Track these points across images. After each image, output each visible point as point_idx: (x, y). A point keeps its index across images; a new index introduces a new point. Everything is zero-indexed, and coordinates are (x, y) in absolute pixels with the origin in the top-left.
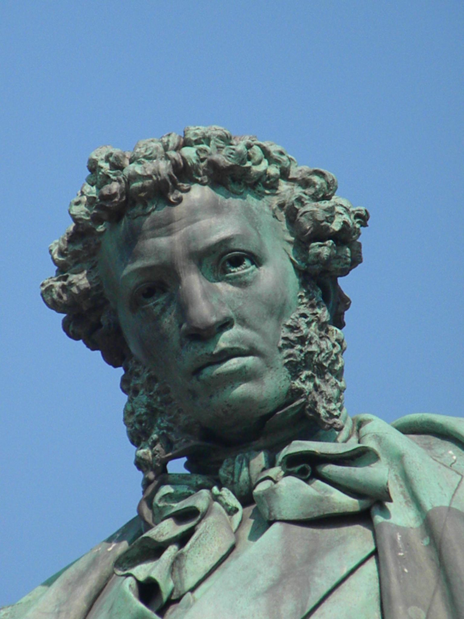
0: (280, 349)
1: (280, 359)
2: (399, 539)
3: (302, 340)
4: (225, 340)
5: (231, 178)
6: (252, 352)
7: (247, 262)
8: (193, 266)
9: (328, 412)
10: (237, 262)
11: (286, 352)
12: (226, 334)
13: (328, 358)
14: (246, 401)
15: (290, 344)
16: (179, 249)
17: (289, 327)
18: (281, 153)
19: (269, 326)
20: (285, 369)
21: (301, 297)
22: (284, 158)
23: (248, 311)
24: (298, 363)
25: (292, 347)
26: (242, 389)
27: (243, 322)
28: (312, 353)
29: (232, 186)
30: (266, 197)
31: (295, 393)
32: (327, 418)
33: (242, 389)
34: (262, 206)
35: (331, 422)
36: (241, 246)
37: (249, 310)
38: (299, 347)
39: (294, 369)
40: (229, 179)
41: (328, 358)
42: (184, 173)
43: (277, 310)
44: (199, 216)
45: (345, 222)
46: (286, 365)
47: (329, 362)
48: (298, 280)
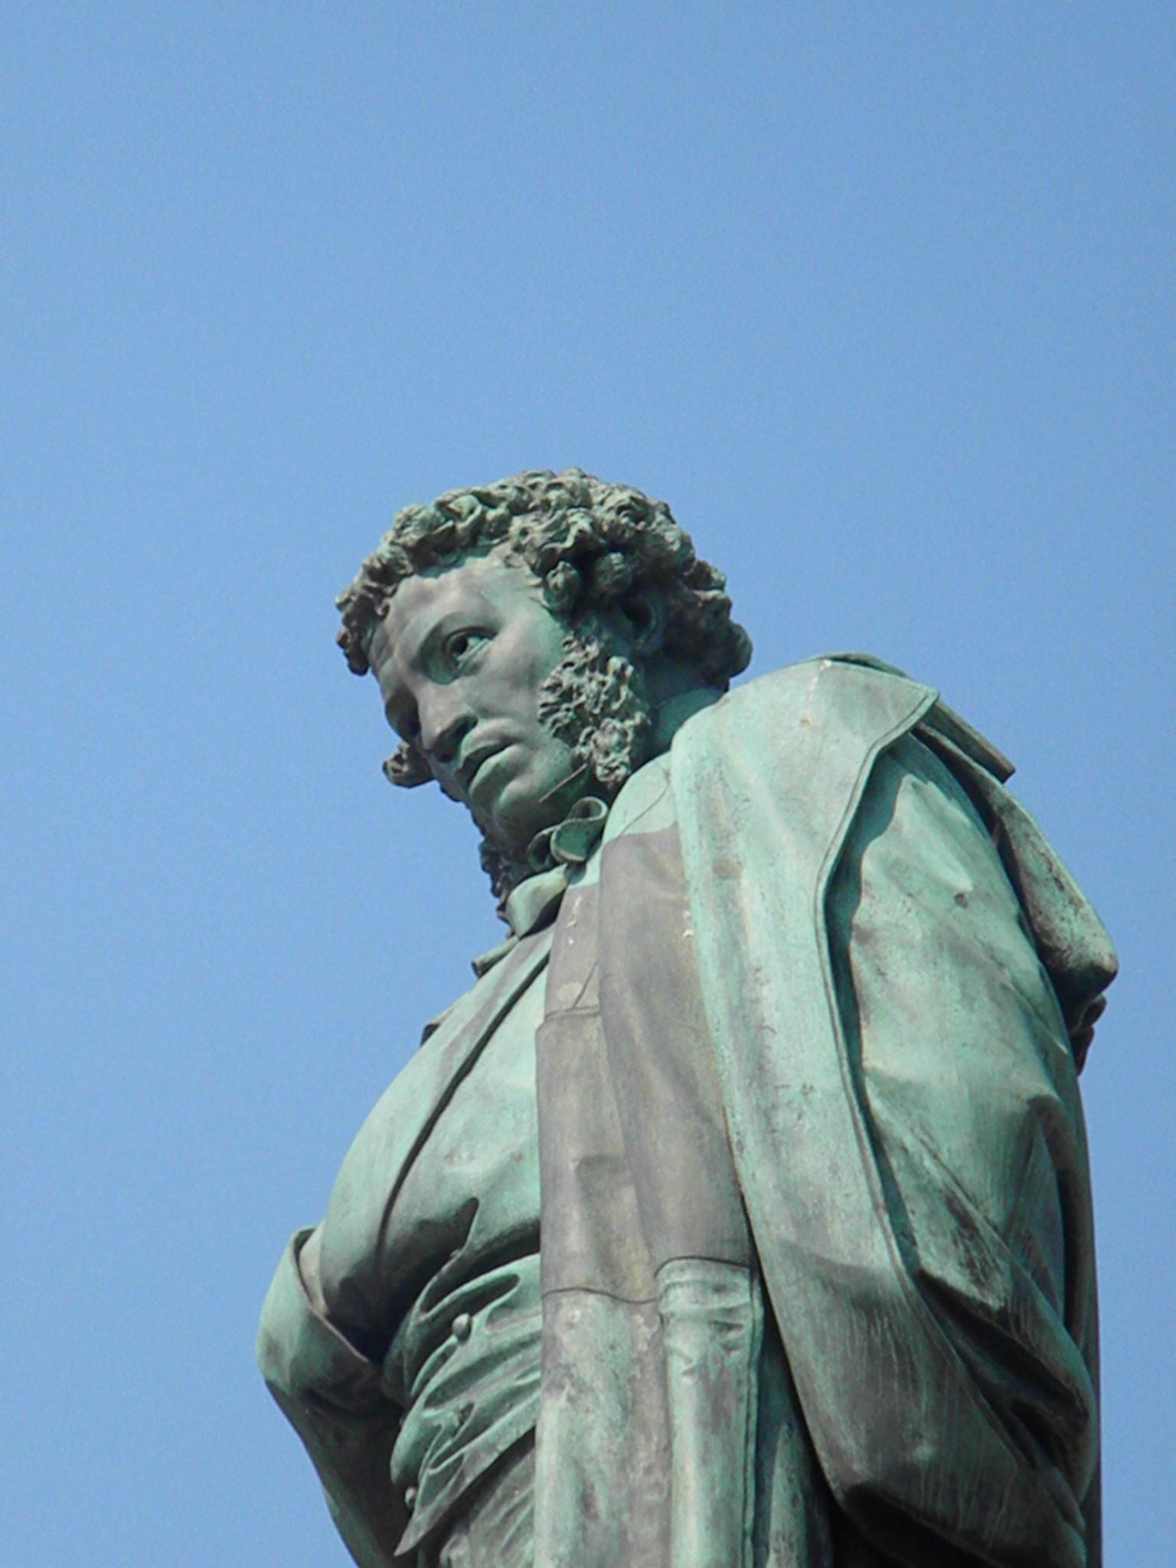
0: (542, 721)
1: (545, 731)
2: (577, 903)
3: (568, 695)
4: (468, 745)
5: (438, 547)
6: (505, 742)
7: (472, 641)
8: (420, 676)
9: (606, 767)
10: (462, 646)
11: (550, 720)
12: (468, 739)
13: (596, 704)
14: (518, 802)
15: (552, 709)
16: (401, 665)
17: (548, 688)
18: (503, 487)
19: (520, 701)
20: (557, 740)
21: (568, 643)
22: (508, 491)
23: (488, 698)
24: (567, 726)
25: (557, 710)
26: (514, 787)
27: (487, 713)
28: (581, 706)
29: (442, 561)
30: (496, 549)
31: (578, 760)
32: (607, 775)
33: (514, 787)
34: (483, 567)
35: (612, 777)
36: (457, 627)
37: (489, 696)
38: (565, 706)
39: (568, 734)
40: (433, 554)
41: (596, 704)
42: (385, 575)
43: (527, 675)
44: (407, 616)
45: (580, 531)
46: (555, 735)
47: (600, 705)
48: (558, 625)
